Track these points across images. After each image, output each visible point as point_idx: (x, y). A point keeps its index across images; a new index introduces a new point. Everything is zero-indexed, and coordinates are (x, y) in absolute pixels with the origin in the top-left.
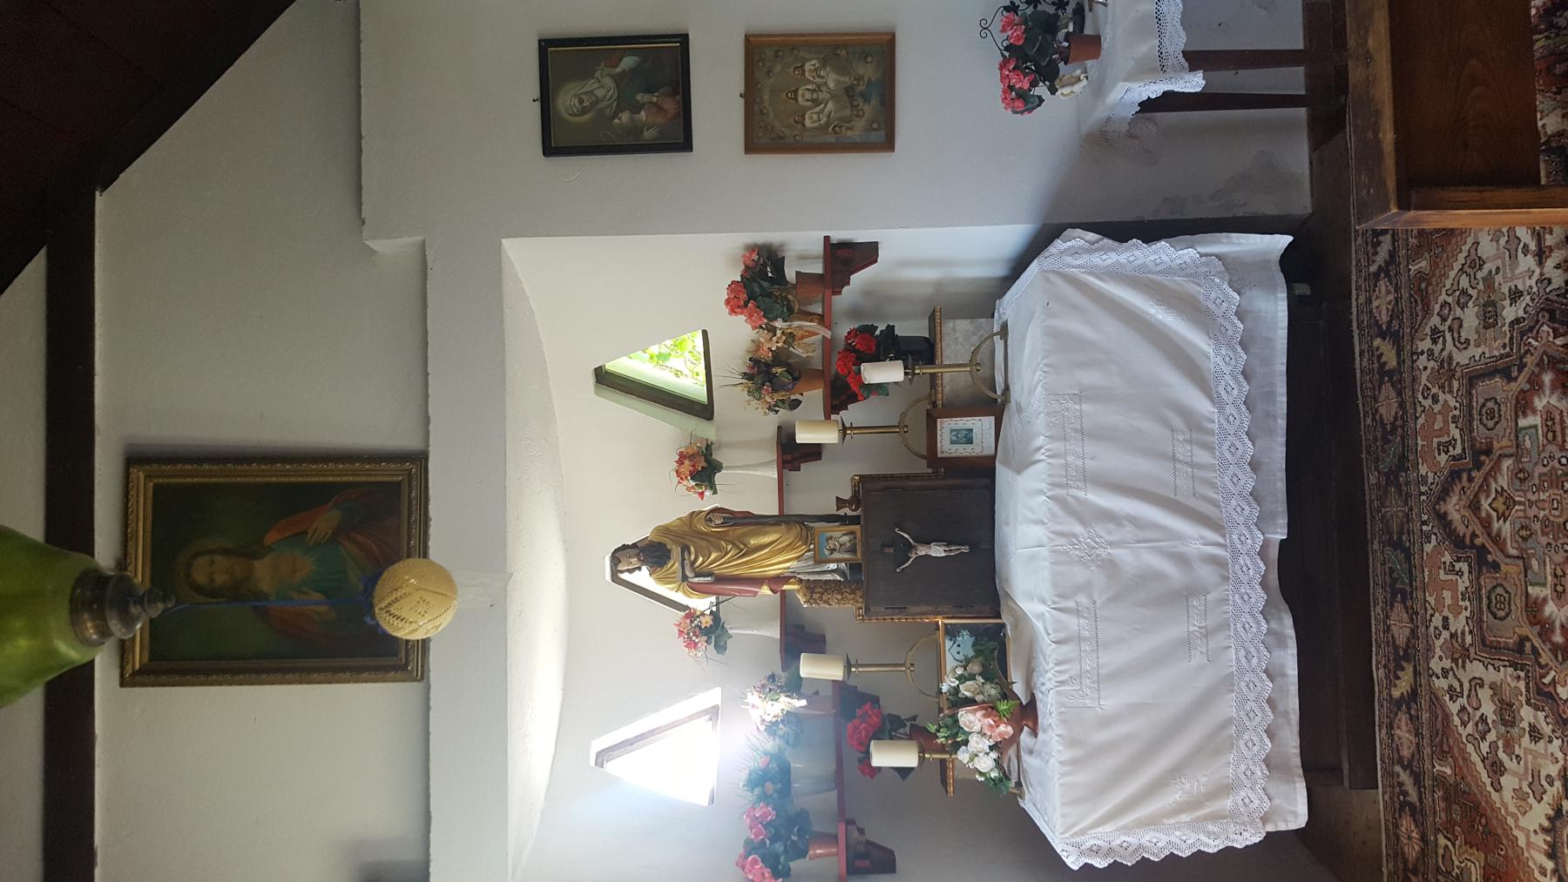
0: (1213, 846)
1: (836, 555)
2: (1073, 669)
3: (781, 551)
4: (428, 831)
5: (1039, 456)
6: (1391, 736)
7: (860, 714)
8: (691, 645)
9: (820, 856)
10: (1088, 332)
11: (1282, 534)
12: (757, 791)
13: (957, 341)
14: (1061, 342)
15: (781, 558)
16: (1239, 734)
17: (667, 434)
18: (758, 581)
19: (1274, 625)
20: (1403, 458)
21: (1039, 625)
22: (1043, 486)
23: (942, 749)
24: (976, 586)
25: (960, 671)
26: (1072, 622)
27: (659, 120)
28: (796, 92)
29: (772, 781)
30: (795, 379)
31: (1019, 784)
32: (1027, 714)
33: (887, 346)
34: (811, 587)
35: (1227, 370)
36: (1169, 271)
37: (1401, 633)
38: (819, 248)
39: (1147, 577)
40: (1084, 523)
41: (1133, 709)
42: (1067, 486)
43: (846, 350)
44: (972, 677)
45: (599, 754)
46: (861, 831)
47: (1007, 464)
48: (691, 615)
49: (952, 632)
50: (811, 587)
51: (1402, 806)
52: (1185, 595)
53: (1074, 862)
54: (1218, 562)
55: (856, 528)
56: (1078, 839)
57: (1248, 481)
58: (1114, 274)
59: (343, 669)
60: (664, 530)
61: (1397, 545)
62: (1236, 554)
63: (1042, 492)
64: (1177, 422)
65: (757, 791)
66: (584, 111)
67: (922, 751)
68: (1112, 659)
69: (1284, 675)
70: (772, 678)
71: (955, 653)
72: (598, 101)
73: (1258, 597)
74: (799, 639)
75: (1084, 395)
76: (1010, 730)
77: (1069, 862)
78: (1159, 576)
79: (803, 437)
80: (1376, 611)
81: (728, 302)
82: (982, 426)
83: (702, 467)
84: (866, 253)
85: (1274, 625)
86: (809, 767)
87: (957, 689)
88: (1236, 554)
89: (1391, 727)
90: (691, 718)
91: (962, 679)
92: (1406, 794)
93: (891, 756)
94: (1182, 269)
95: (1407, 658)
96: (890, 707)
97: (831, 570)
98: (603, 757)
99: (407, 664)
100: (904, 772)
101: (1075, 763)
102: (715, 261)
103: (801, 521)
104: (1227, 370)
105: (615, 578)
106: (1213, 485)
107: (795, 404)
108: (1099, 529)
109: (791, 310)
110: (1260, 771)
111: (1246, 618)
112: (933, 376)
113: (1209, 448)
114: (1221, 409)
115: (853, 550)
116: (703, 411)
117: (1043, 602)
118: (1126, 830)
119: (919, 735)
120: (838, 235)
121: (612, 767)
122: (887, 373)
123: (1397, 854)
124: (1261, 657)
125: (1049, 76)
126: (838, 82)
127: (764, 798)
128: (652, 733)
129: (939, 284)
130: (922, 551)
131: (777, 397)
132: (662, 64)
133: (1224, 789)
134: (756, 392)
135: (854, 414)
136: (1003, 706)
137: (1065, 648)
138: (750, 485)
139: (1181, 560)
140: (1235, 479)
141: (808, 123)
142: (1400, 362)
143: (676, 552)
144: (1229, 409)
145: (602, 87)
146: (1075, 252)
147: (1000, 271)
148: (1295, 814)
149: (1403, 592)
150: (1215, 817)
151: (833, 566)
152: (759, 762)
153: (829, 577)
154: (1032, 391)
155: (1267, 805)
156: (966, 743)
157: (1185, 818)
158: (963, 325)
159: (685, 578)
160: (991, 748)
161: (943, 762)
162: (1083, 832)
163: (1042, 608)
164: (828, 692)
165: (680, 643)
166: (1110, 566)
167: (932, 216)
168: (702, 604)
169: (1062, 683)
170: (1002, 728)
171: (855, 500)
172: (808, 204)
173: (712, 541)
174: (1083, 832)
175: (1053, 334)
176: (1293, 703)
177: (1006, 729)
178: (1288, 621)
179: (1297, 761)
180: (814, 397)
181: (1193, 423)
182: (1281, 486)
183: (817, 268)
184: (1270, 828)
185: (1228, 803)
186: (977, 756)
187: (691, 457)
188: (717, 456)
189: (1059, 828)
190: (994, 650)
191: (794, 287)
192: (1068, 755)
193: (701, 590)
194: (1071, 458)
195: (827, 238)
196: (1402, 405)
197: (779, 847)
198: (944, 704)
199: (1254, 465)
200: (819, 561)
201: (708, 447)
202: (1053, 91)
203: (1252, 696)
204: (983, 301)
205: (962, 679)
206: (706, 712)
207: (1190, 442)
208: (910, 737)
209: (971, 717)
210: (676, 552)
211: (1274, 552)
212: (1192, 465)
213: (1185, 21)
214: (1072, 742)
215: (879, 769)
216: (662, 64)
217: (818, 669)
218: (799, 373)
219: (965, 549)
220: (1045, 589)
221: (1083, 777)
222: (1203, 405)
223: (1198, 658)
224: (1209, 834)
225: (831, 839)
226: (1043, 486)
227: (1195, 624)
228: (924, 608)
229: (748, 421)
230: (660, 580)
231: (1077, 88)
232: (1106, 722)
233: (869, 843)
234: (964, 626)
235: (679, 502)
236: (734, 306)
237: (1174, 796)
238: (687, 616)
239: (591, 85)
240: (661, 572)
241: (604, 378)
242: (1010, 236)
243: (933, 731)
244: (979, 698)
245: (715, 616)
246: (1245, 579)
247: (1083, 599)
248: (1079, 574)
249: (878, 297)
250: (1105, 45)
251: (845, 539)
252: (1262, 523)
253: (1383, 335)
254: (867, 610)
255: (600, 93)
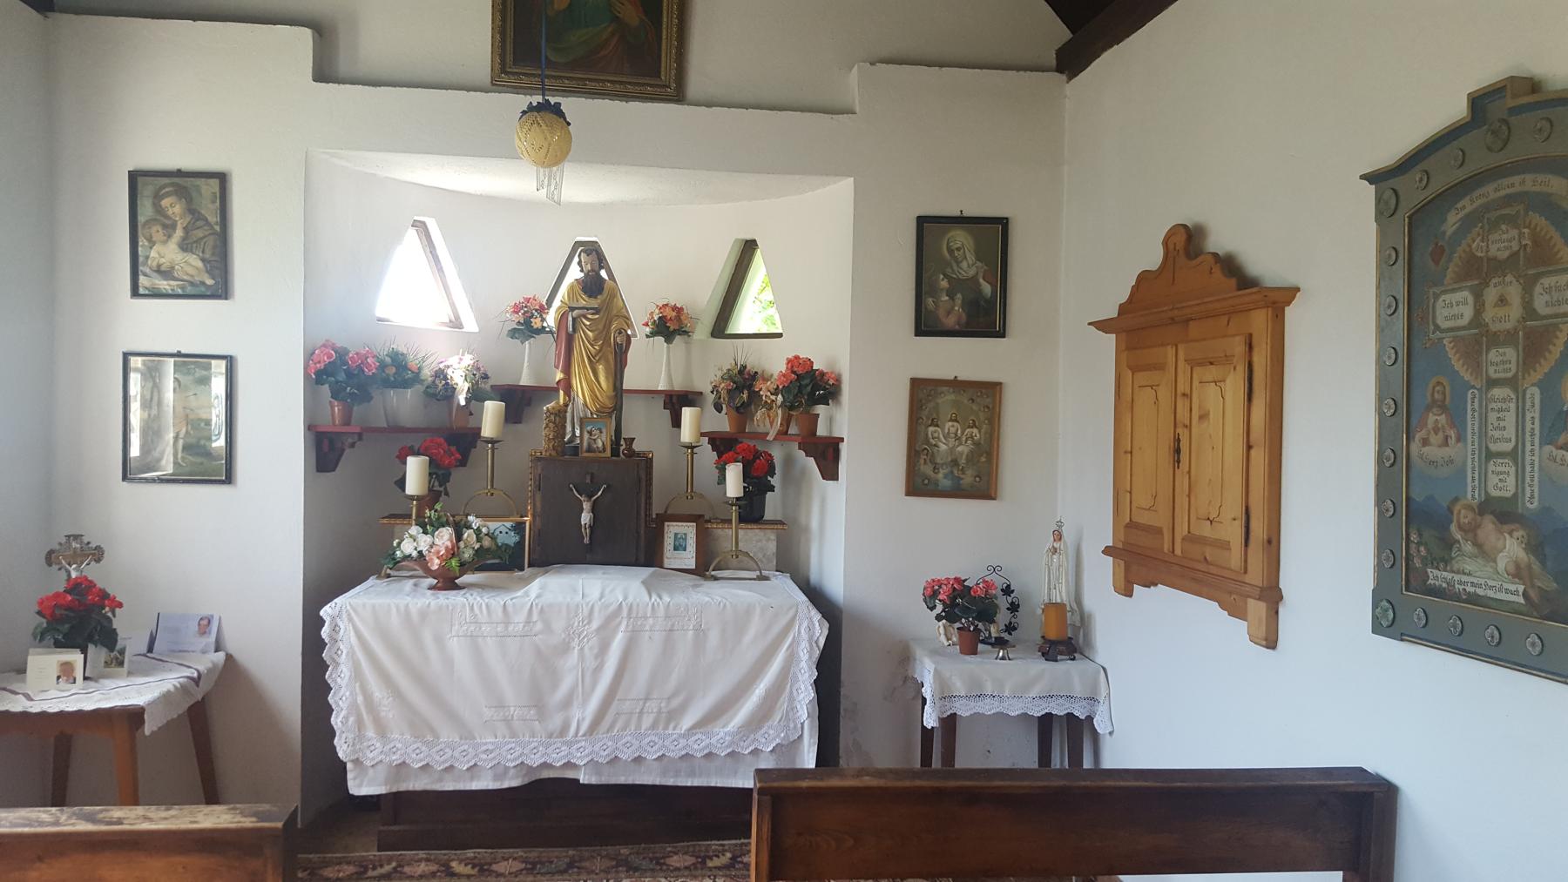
0: (336, 721)
1: (586, 436)
2: (483, 617)
3: (592, 390)
4: (364, 84)
5: (654, 597)
6: (420, 860)
7: (453, 444)
8: (517, 309)
9: (332, 408)
10: (748, 638)
11: (584, 778)
12: (388, 360)
13: (759, 542)
14: (742, 618)
15: (585, 390)
16: (426, 743)
17: (702, 298)
18: (567, 370)
19: (512, 772)
20: (636, 869)
21: (520, 593)
22: (630, 599)
23: (420, 515)
24: (554, 548)
25: (484, 530)
26: (521, 617)
27: (941, 313)
28: (974, 426)
29: (398, 371)
30: (737, 409)
31: (389, 576)
32: (447, 581)
33: (757, 484)
34: (560, 414)
35: (714, 741)
36: (792, 699)
37: (501, 867)
38: (836, 435)
39: (555, 677)
40: (598, 630)
41: (448, 662)
42: (629, 617)
43: (757, 452)
44: (479, 540)
45: (424, 223)
46: (352, 445)
47: (652, 575)
48: (542, 310)
49: (519, 528)
50: (560, 414)
51: (363, 867)
52: (538, 704)
53: (322, 613)
54: (563, 731)
55: (608, 453)
56: (344, 616)
57: (626, 755)
58: (792, 658)
59: (504, 20)
60: (614, 293)
61: (570, 865)
62: (570, 744)
63: (625, 598)
64: (675, 703)
65: (388, 360)
66: (951, 251)
67: (419, 498)
68: (490, 648)
69: (472, 779)
70: (485, 377)
71: (501, 529)
72: (958, 263)
73: (535, 761)
74: (518, 401)
75: (700, 633)
76: (435, 567)
77: (327, 608)
78: (555, 686)
79: (687, 413)
80: (520, 852)
81: (797, 358)
82: (688, 559)
83: (669, 326)
84: (830, 473)
85: (512, 772)
86: (404, 405)
87: (469, 527)
88: (570, 744)
89: (428, 860)
90: (453, 305)
91: (478, 532)
92: (374, 868)
93: (415, 472)
94: (792, 708)
95: (482, 871)
96: (457, 475)
97: (572, 430)
98: (421, 227)
99: (507, 73)
100: (401, 483)
101: (406, 615)
102: (828, 348)
103: (617, 408)
104: (714, 741)
105: (578, 244)
106: (624, 728)
107: (718, 408)
108: (594, 641)
109: (791, 408)
110: (396, 759)
111: (519, 750)
112: (730, 521)
113: (654, 726)
114: (683, 736)
115: (590, 450)
116: (720, 328)
117: (538, 596)
118: (352, 654)
119: (431, 498)
120: (844, 447)
121: (412, 235)
122: (734, 483)
123: (327, 864)
124: (486, 761)
125: (949, 615)
126: (961, 454)
127: (383, 366)
128: (440, 270)
129: (807, 529)
130: (586, 506)
131: (724, 394)
132: (986, 318)
133: (382, 731)
134: (728, 376)
135: (707, 455)
136: (454, 562)
137: (500, 611)
138: (651, 367)
139: (567, 703)
140: (628, 745)
141: (931, 429)
142: (710, 869)
143: (594, 303)
144: (683, 742)
145: (969, 266)
146: (810, 629)
147: (814, 577)
148: (360, 786)
149: (533, 868)
150: (360, 723)
151: (578, 433)
152: (413, 363)
153: (569, 428)
154: (707, 594)
155: (368, 763)
156: (425, 532)
157: (360, 699)
158: (772, 547)
159: (572, 309)
160: (420, 552)
161: (410, 516)
162: (350, 620)
163: (533, 595)
164: (472, 424)
165: (519, 299)
166: (565, 648)
167: (862, 530)
168: (551, 320)
169: (472, 608)
170: (437, 561)
171: (632, 454)
172: (869, 426)
173: (603, 333)
174: (350, 620)
175: (749, 611)
176: (449, 786)
177: (435, 564)
178: (515, 783)
179: (403, 787)
180: (721, 423)
181: (673, 716)
182: (622, 780)
183: (821, 431)
184: (349, 766)
185: (370, 733)
186: (414, 541)
187: (678, 318)
188: (678, 339)
189: (353, 601)
190: (504, 561)
191: (808, 413)
192: (414, 610)
193: (562, 320)
194: (651, 621)
195: (842, 440)
196: (677, 869)
197: (342, 377)
198: (458, 518)
199: (638, 760)
200: (582, 422)
201: (686, 333)
202: (939, 618)
203: (456, 754)
204: (791, 564)
205: (478, 532)
206: (457, 318)
207: (660, 712)
208: (430, 490)
209: (446, 537)
210: (594, 303)
211: (570, 775)
212: (641, 712)
213: (977, 716)
214: (424, 614)
215: (405, 463)
216: (986, 318)
217: (491, 415)
218: (743, 412)
219: (586, 540)
220: (548, 598)
221: (395, 621)
222: (687, 722)
223: (488, 713)
224: (346, 718)
225: (347, 421)
226: (630, 599)
227: (515, 712)
228: (538, 504)
229: (705, 366)
230: (572, 287)
231: (943, 638)
232: (439, 641)
233: (343, 450)
234: (523, 537)
235: (640, 307)
236: (794, 362)
237: (379, 693)
238: (541, 306)
239: (971, 258)
240: (578, 289)
241: (749, 247)
242: (836, 584)
243: (432, 508)
244: (462, 544)
245: (542, 330)
246: (549, 750)
247: (539, 626)
248: (558, 625)
249: (795, 480)
250: (968, 658)
251: (600, 444)
252: (592, 763)
253: (734, 858)
254: (539, 459)
255: (964, 265)
